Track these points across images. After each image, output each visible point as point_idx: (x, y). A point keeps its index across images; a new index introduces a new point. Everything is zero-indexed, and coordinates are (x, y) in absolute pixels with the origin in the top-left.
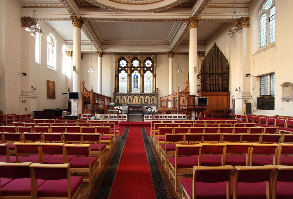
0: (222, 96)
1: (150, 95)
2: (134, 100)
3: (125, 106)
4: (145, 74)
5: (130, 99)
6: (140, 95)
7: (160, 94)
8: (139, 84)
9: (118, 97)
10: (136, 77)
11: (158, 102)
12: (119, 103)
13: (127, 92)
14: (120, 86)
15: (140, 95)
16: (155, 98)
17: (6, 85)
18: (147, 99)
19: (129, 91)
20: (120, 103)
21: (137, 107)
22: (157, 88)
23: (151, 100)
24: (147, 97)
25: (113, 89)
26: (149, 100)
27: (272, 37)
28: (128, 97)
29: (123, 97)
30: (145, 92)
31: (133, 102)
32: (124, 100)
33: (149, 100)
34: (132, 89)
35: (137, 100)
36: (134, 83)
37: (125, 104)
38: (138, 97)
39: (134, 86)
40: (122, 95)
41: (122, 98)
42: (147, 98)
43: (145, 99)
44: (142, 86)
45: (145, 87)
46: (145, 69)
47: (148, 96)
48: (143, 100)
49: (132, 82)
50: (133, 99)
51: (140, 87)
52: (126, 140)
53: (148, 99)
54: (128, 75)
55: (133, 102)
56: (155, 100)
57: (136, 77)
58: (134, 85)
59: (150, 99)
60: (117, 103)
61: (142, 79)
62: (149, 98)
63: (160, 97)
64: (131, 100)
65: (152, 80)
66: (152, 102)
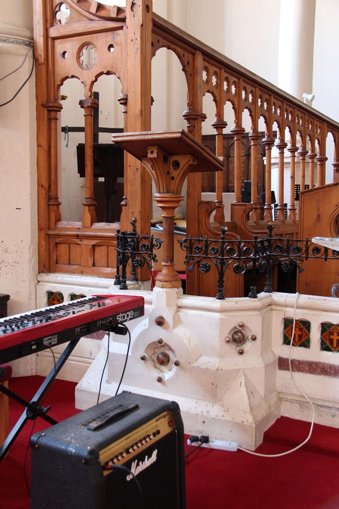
23: (289, 146)
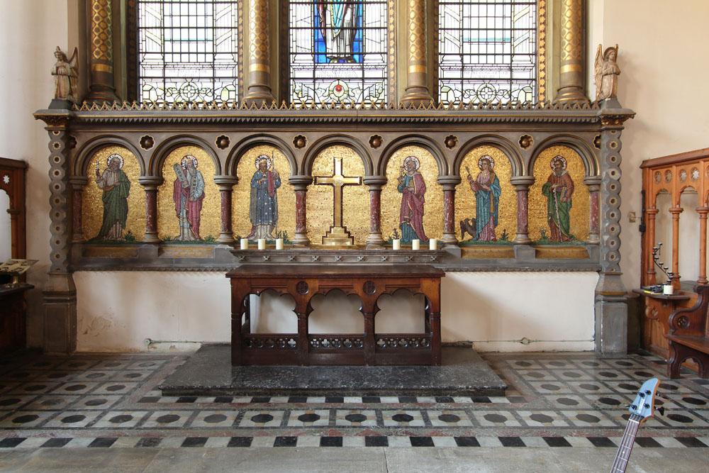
1: (514, 137)
2: (311, 201)
3: (198, 266)
5: (266, 184)
6: (388, 138)
7: (644, 128)
9: (114, 166)
11: (624, 211)
12: (131, 239)
13: (228, 94)
14: (149, 42)
15: (388, 138)
16: (574, 166)
17: (473, 447)
18: (477, 187)
19: (251, 94)
20: (143, 234)
21: (358, 288)
22: (597, 41)
23: (536, 192)
24: (486, 163)
25: (52, 62)
26: (508, 196)
28: (248, 166)
29: (177, 157)
30: (449, 95)
31: (302, 221)
32: (188, 196)
33: (508, 196)
34: (301, 65)
35: (358, 200)
37: (197, 251)
38: (367, 159)
39: (320, 41)
40: (159, 138)
41: (170, 175)
42: (475, 172)
43: (451, 187)
44: (421, 42)
45: (448, 45)
47: (490, 152)
48: (434, 199)
50: (304, 182)
51: (397, 42)
53: (494, 180)
55: (302, 221)
56: (581, 197)
58: (319, 26)
59: (524, 188)
60: (104, 231)
62: (503, 169)
63: (636, 162)
64: (286, 198)
66: (539, 222)
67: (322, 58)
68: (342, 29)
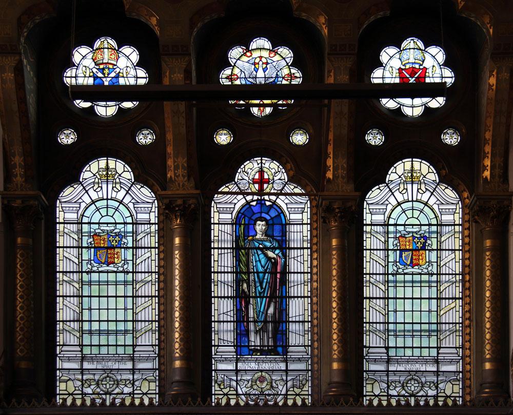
0: (66, 382)
4: (375, 194)
8: (298, 309)
10: (260, 226)
13: (332, 100)
19: (174, 390)
27: (425, 305)
36: (241, 298)
39: (241, 334)
46: (375, 139)
49: (216, 290)
52: (149, 178)
54: (167, 211)
57: (260, 226)
58: (241, 319)
61: (341, 249)
65: (453, 263)
67: (245, 350)
68: (265, 322)
